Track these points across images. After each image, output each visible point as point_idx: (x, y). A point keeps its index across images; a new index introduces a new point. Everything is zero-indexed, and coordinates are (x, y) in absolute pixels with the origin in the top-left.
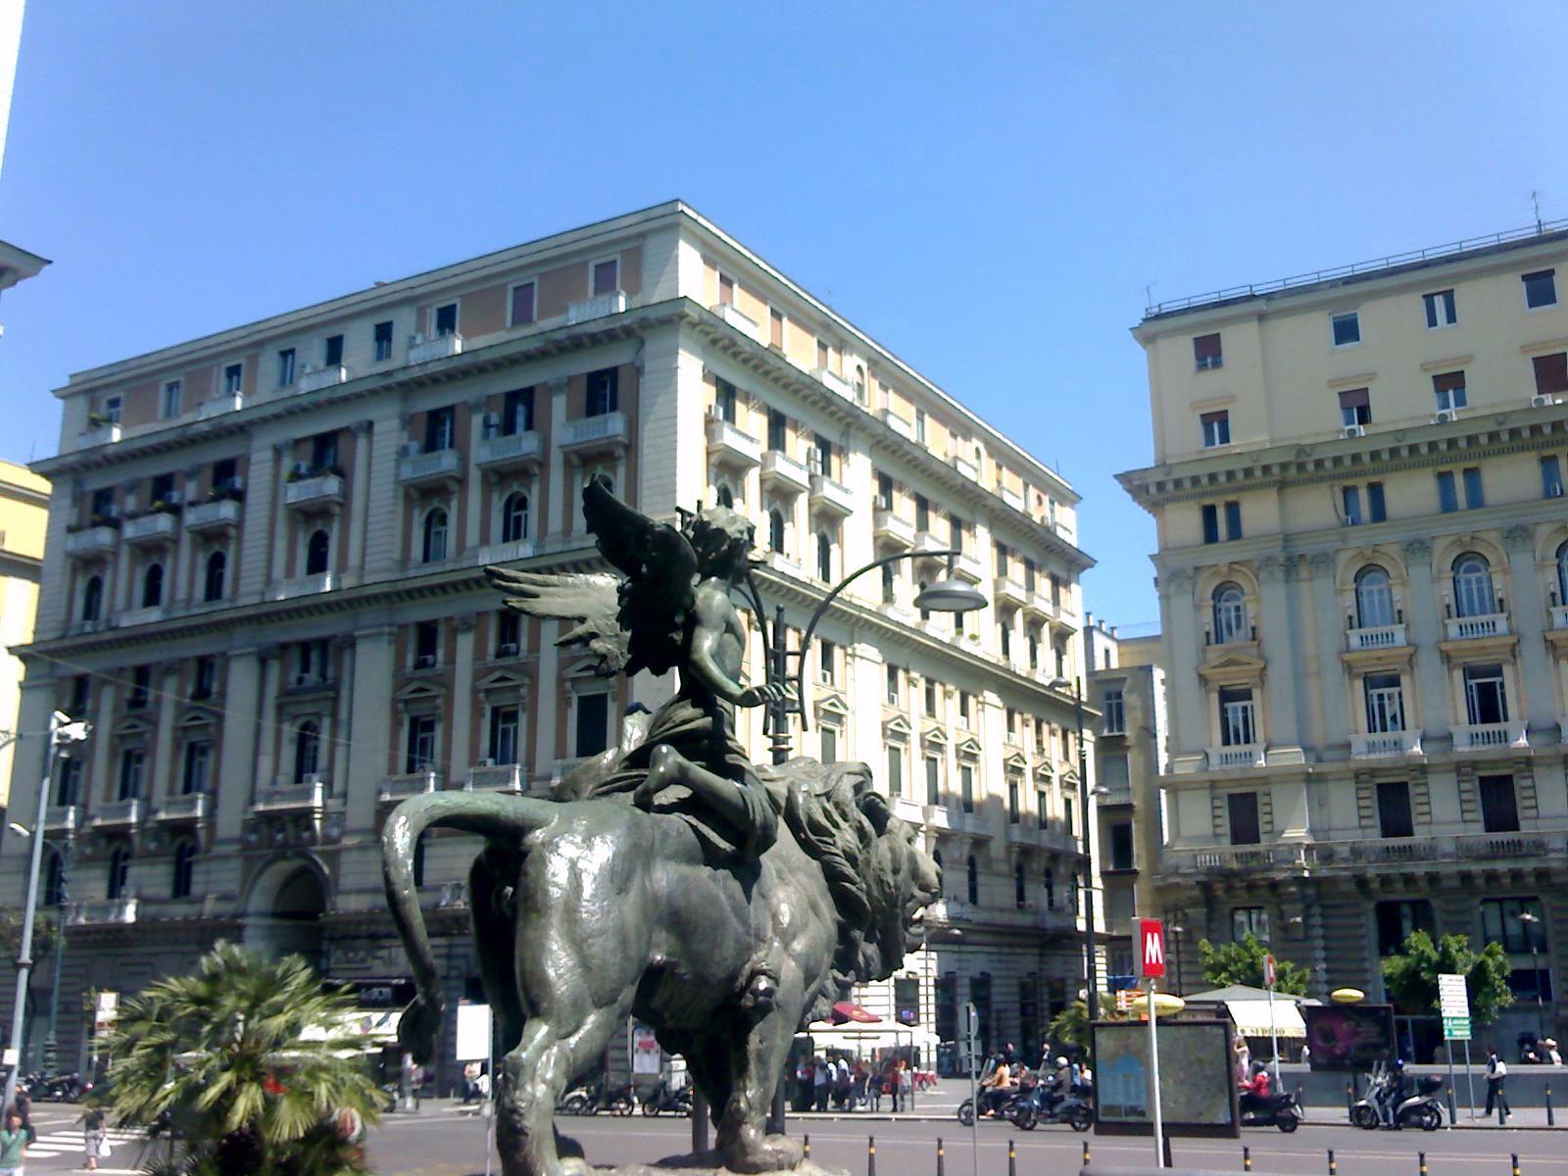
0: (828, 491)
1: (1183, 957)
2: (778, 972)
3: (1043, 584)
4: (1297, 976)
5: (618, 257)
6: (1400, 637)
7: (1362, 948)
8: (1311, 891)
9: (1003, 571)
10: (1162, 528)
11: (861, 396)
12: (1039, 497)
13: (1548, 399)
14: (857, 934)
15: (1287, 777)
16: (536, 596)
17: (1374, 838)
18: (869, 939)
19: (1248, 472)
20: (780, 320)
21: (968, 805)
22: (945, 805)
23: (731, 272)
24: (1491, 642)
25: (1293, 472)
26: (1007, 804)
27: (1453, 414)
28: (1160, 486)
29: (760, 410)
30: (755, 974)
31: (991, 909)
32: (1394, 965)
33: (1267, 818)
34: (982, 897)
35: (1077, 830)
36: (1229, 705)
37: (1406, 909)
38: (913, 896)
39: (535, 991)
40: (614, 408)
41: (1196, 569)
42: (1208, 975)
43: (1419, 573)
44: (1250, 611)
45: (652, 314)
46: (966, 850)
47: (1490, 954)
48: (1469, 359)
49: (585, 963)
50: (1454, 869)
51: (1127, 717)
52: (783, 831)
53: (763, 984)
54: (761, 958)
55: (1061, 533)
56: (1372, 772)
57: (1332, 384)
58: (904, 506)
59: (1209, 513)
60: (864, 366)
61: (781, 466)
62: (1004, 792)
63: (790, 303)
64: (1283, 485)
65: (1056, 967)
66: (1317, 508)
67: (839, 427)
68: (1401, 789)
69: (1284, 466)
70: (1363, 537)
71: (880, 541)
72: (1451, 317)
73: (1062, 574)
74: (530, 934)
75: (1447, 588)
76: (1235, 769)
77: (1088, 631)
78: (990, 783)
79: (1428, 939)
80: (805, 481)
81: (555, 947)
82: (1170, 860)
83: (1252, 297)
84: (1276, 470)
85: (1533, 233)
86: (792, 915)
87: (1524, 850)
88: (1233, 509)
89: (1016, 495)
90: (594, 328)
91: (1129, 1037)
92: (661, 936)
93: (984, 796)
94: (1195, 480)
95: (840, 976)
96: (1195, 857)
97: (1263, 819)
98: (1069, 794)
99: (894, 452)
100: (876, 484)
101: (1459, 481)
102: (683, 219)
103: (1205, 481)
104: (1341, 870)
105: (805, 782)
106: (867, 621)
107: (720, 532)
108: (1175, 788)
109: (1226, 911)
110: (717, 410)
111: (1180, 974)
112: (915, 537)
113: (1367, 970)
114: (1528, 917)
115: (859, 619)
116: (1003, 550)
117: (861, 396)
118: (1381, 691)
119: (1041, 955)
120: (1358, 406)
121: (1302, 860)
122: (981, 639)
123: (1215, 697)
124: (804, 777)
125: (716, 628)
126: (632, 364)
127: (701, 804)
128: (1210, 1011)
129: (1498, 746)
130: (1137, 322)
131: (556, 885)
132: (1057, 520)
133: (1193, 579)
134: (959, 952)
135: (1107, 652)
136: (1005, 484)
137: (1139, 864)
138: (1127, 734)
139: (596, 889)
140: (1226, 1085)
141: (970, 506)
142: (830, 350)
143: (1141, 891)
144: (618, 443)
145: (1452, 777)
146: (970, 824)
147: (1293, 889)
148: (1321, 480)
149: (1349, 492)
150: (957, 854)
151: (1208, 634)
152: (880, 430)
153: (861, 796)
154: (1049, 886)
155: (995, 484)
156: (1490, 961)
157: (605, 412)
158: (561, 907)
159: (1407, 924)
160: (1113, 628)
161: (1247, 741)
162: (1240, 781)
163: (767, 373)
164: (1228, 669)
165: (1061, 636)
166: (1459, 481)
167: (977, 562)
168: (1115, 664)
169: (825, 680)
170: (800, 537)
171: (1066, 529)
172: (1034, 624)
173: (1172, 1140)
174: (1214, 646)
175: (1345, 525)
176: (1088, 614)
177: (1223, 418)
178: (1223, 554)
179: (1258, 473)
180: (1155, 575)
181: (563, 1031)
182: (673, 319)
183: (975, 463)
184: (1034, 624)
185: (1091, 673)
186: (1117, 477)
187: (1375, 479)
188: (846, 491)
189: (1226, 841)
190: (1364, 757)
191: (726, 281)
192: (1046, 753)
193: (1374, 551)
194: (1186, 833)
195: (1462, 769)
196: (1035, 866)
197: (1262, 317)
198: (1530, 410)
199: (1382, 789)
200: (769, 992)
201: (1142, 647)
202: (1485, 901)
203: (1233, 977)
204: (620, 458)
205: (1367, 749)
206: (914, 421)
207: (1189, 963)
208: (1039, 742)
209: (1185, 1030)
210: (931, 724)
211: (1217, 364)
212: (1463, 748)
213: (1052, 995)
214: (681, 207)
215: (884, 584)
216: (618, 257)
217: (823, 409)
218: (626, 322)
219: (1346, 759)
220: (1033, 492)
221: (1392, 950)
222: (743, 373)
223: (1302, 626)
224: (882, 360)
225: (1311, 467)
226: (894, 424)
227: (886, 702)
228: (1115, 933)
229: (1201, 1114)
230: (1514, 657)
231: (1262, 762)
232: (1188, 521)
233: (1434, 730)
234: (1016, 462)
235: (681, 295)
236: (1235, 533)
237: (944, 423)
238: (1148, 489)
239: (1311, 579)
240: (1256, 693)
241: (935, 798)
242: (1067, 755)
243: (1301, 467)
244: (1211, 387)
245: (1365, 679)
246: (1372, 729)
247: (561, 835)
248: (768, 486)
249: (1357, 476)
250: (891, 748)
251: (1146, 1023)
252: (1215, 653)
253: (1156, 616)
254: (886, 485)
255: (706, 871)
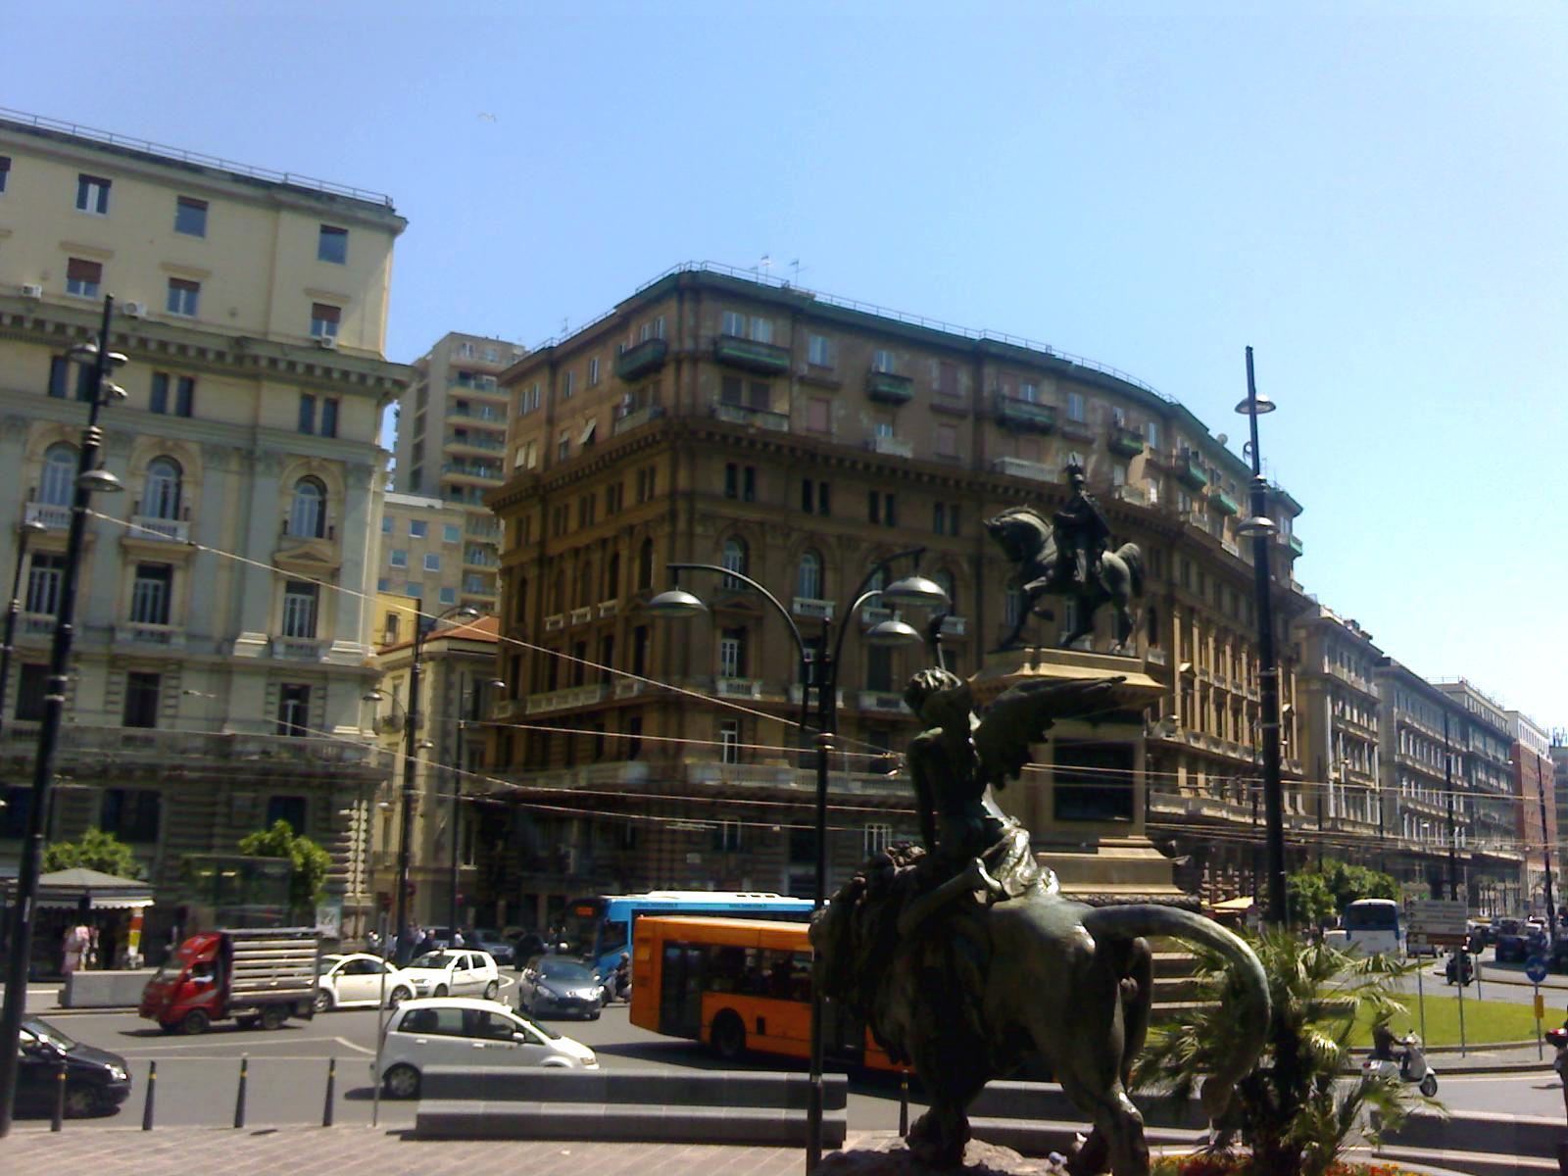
48: (207, 274)
57: (65, 246)
68: (153, 679)
72: (102, 206)
101: (320, 406)
166: (320, 406)
177: (193, 287)
199: (134, 677)
244: (330, 278)
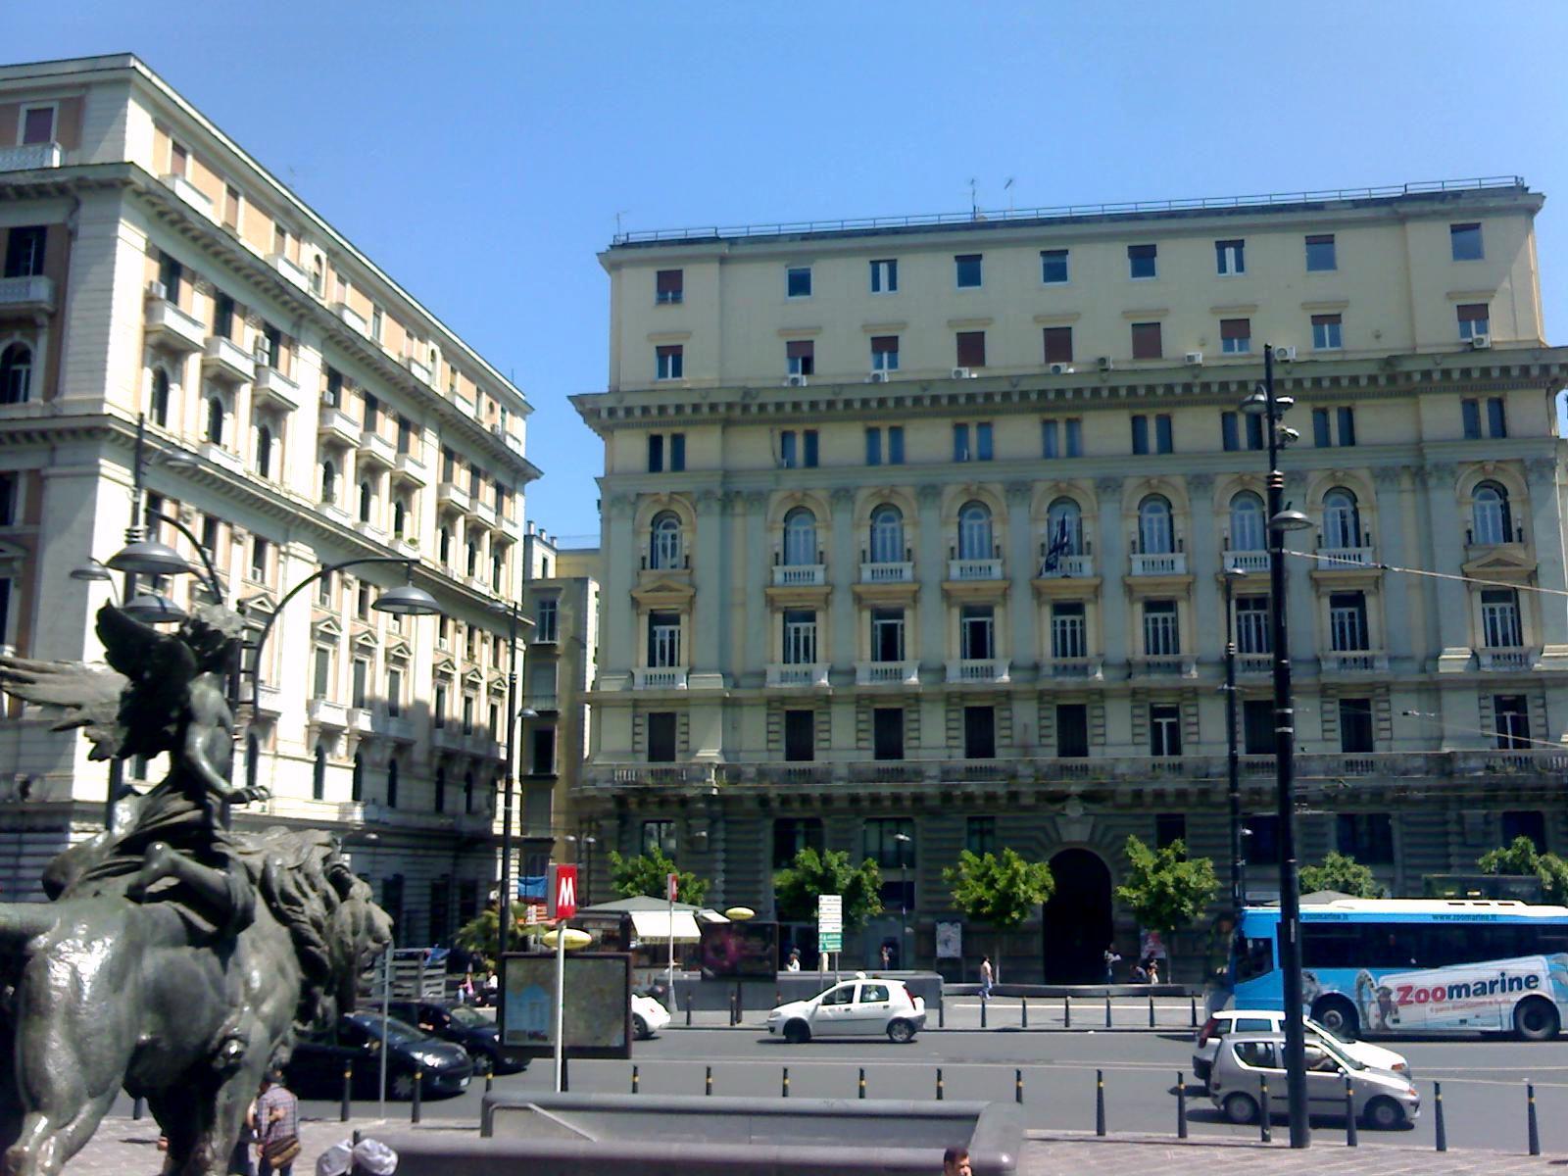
0: (274, 383)
1: (594, 866)
2: (248, 1035)
3: (488, 493)
4: (696, 886)
5: (56, 106)
6: (820, 577)
7: (758, 862)
8: (717, 808)
9: (448, 476)
10: (610, 454)
11: (317, 287)
12: (491, 407)
13: (966, 373)
14: (318, 990)
15: (706, 700)
16: (32, 682)
17: (779, 761)
18: (327, 993)
19: (696, 408)
20: (236, 199)
21: (392, 710)
22: (370, 708)
23: (185, 139)
24: (898, 587)
25: (737, 412)
26: (433, 710)
27: (886, 375)
28: (612, 412)
29: (207, 293)
30: (226, 1040)
31: (403, 812)
32: (783, 878)
33: (683, 737)
34: (400, 801)
35: (501, 736)
36: (658, 629)
37: (800, 827)
38: (367, 948)
39: (37, 1087)
40: (38, 271)
41: (639, 495)
42: (615, 885)
43: (842, 518)
44: (686, 540)
45: (91, 175)
46: (388, 754)
47: (866, 869)
49: (83, 1061)
50: (843, 791)
51: (559, 627)
52: (261, 909)
53: (234, 1048)
54: (235, 1023)
55: (510, 443)
56: (783, 699)
58: (353, 405)
59: (655, 443)
60: (324, 256)
61: (225, 353)
62: (429, 696)
63: (248, 182)
64: (727, 424)
65: (469, 870)
66: (756, 448)
67: (291, 318)
69: (730, 406)
70: (796, 480)
71: (325, 439)
72: (893, 286)
73: (506, 483)
74: (33, 1035)
75: (865, 534)
76: (657, 690)
77: (528, 539)
78: (418, 688)
79: (814, 854)
80: (251, 373)
81: (54, 1045)
82: (588, 773)
83: (716, 240)
84: (722, 409)
85: (967, 218)
86: (263, 982)
87: (905, 777)
88: (678, 441)
89: (468, 402)
90: (21, 180)
91: (536, 969)
92: (149, 1017)
93: (411, 701)
94: (645, 410)
95: (300, 1027)
96: (613, 771)
97: (679, 738)
98: (496, 701)
99: (346, 348)
100: (325, 379)
101: (885, 438)
102: (135, 76)
103: (654, 412)
104: (746, 789)
105: (278, 854)
106: (304, 519)
107: (217, 632)
108: (598, 706)
109: (638, 824)
110: (159, 290)
111: (589, 882)
112: (361, 438)
113: (760, 882)
114: (902, 837)
115: (296, 517)
116: (449, 455)
117: (317, 287)
118: (797, 625)
119: (456, 857)
120: (803, 357)
121: (712, 779)
122: (420, 544)
123: (645, 620)
124: (277, 849)
125: (209, 725)
126: (64, 225)
127: (188, 892)
128: (613, 920)
129: (894, 682)
130: (604, 247)
131: (58, 988)
132: (507, 429)
133: (635, 505)
134: (374, 854)
135: (545, 561)
136: (458, 389)
137: (557, 770)
138: (558, 642)
139: (96, 991)
140: (623, 1012)
141: (417, 408)
142: (288, 236)
143: (557, 796)
144: (41, 310)
145: (852, 708)
146: (394, 728)
147: (701, 805)
148: (762, 422)
149: (786, 436)
150: (378, 758)
151: (644, 559)
152: (334, 324)
153: (328, 865)
154: (468, 790)
155: (448, 389)
156: (865, 875)
157: (27, 273)
158: (62, 1010)
159: (800, 840)
160: (553, 538)
161: (671, 664)
162: (663, 702)
163: (217, 254)
164: (660, 594)
165: (501, 545)
166: (885, 438)
167: (423, 467)
168: (551, 574)
169: (255, 577)
170: (240, 429)
171: (515, 439)
172: (475, 531)
173: (569, 1061)
174: (648, 571)
175: (780, 467)
176: (530, 523)
177: (676, 352)
178: (665, 483)
179: (705, 410)
180: (599, 497)
181: (61, 1122)
182: (117, 183)
183: (430, 367)
184: (475, 531)
185: (527, 580)
186: (569, 397)
187: (810, 427)
188: (294, 385)
189: (644, 757)
190: (777, 686)
191: (179, 150)
192: (477, 660)
193: (805, 495)
194: (606, 748)
195: (860, 700)
196: (456, 770)
197: (723, 260)
198: (949, 380)
200: (238, 1055)
201: (582, 559)
202: (869, 821)
203: (638, 887)
204: (42, 326)
205: (782, 679)
206: (370, 318)
207: (598, 872)
208: (470, 649)
209: (590, 963)
210: (362, 627)
211: (677, 299)
212: (864, 682)
213: (464, 897)
214: (133, 63)
215: (325, 483)
216: (56, 106)
217: (275, 297)
218: (60, 179)
219: (762, 686)
220: (485, 399)
221: (784, 863)
222: (189, 250)
223: (733, 555)
224: (342, 251)
225: (754, 409)
226: (349, 319)
227: (318, 603)
228: (529, 836)
229: (598, 1038)
230: (915, 601)
231: (683, 685)
232: (634, 448)
233: (842, 665)
234: (472, 369)
235: (127, 159)
236: (678, 463)
237: (401, 323)
238: (601, 414)
239: (744, 515)
240: (684, 619)
241: (359, 702)
242: (501, 663)
243: (746, 408)
244: (669, 321)
245: (785, 614)
246: (786, 661)
247: (61, 938)
248: (210, 373)
249: (795, 420)
250: (319, 649)
251: (553, 956)
252: (649, 578)
253: (596, 528)
254: (335, 380)
255: (187, 951)
